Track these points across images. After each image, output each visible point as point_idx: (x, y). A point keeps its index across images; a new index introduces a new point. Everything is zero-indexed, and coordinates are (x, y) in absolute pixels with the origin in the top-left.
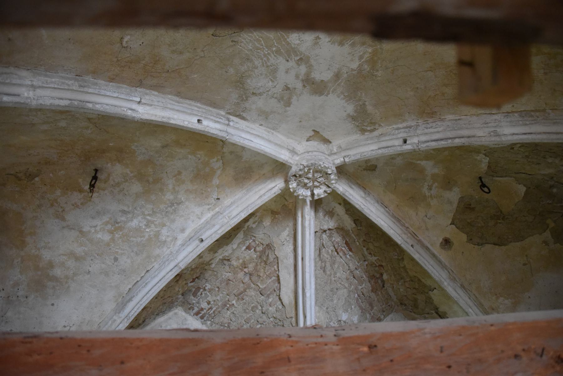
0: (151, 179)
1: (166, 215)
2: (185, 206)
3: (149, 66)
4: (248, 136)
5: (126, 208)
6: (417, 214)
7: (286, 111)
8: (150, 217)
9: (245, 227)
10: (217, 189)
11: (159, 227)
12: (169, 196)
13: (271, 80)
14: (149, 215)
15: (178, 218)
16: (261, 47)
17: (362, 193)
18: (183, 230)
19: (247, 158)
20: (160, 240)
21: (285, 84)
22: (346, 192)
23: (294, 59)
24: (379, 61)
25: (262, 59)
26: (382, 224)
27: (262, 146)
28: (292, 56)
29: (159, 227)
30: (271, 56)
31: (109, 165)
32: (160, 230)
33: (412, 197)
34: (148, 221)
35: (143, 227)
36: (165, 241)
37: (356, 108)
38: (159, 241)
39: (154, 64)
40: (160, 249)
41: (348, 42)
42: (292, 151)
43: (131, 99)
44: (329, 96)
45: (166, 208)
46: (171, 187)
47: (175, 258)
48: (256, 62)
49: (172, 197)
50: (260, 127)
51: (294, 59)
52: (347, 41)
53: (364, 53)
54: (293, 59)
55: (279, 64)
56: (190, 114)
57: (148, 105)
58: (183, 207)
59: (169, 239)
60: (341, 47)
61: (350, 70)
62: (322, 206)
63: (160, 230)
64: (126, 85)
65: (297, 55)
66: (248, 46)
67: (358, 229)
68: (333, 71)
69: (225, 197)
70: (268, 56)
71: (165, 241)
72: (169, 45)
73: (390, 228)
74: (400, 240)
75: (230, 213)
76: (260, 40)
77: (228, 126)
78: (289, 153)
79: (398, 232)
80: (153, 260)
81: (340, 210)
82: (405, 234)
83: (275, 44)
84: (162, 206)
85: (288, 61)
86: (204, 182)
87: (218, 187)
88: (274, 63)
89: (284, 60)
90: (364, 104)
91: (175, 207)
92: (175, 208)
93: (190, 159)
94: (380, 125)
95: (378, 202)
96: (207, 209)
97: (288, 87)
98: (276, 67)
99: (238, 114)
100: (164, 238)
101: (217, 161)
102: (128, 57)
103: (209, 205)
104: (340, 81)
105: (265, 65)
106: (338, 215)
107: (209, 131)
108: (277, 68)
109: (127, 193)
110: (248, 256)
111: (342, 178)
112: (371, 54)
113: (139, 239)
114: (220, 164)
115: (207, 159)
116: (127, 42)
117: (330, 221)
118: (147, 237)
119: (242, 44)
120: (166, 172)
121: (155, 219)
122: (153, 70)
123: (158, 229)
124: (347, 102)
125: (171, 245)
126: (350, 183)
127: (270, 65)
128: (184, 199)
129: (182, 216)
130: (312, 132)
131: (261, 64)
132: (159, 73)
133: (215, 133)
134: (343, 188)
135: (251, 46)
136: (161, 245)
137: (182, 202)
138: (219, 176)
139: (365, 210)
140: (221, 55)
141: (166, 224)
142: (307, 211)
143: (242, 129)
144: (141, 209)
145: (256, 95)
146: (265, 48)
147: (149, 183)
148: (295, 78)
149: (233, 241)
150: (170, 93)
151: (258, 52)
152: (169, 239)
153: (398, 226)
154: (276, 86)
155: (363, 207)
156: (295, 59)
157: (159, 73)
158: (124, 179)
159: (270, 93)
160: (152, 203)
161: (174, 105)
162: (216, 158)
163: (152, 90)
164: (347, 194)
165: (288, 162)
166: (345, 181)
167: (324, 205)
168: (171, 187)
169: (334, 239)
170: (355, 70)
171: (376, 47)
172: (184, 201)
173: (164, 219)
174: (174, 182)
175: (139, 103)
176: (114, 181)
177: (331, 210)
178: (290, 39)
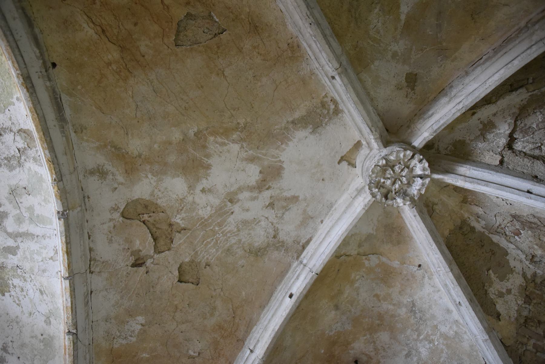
0: (378, 322)
1: (424, 321)
2: (418, 300)
3: (224, 334)
4: (325, 244)
5: (405, 353)
6: (507, 5)
7: (305, 200)
8: (421, 336)
9: (484, 232)
10: (405, 264)
11: (437, 332)
12: (403, 311)
13: (258, 223)
14: (419, 335)
15: (431, 311)
16: (214, 240)
17: (444, 100)
18: (449, 311)
19: (373, 229)
20: (452, 337)
21: (264, 208)
22: (432, 128)
23: (230, 207)
24: (225, 126)
25: (229, 237)
26: (497, 79)
27: (338, 234)
28: (226, 210)
29: (437, 332)
30: (226, 230)
31: (352, 352)
32: (440, 332)
33: (472, 15)
34: (426, 339)
35: (431, 346)
36: (456, 332)
37: (299, 128)
38: (454, 338)
39: (222, 329)
40: (463, 341)
41: (204, 161)
42: (358, 193)
43: (246, 358)
44: (282, 160)
45: (416, 318)
46: (391, 307)
47: (475, 336)
48: (232, 242)
49: (404, 310)
50: (324, 223)
51: (230, 207)
52: (204, 163)
53: (217, 143)
54: (231, 208)
55: (236, 221)
56: (281, 304)
57: (256, 344)
58: (418, 303)
59: (455, 328)
60: (213, 166)
61: (242, 149)
62: (468, 141)
63: (440, 332)
64: (239, 353)
65: (226, 206)
66: (213, 252)
67: (533, 82)
68: (246, 165)
69: (419, 258)
70: (226, 232)
71: (456, 332)
72: (205, 318)
73: (509, 65)
74: (537, 50)
75: (434, 265)
76: (206, 243)
77: (307, 265)
78: (360, 196)
79: (525, 48)
80: (475, 353)
81: (485, 113)
82: (533, 34)
83: (212, 228)
84: (412, 321)
85: (232, 213)
86: (394, 275)
87: (403, 263)
88: (234, 225)
89: (231, 216)
90: (293, 122)
91: (417, 309)
92: (418, 310)
93: (360, 284)
94: (326, 96)
95: (467, 74)
96: (429, 280)
97: (268, 204)
98: (240, 223)
99: (301, 248)
100: (452, 332)
101: (369, 260)
102: (210, 351)
103: (424, 277)
104: (259, 155)
105: (236, 234)
106: (495, 115)
107: (300, 291)
108: (241, 221)
109: (388, 346)
110: (529, 239)
111: (414, 128)
112: (217, 136)
113: (444, 355)
114: (373, 258)
115: (364, 270)
116: (194, 353)
117: (498, 132)
118: (444, 347)
119: (210, 257)
120: (373, 307)
121: (426, 332)
122: (229, 330)
123: (439, 334)
124: (291, 140)
125: (463, 329)
126: (425, 117)
127: (237, 228)
128: (410, 299)
129: (430, 307)
130: (341, 164)
131: (235, 237)
132: (233, 325)
133: (305, 286)
134: (426, 131)
135: (213, 250)
136: (459, 338)
137: (413, 301)
138: (390, 260)
139: (466, 103)
140: (221, 274)
141: (435, 324)
142: (451, 181)
143: (314, 251)
144: (409, 340)
145: (278, 234)
146: (216, 236)
147: (381, 324)
148: (256, 201)
149: (503, 246)
150: (259, 314)
151: (220, 242)
152: (455, 328)
153: (514, 47)
154: (267, 217)
155: (461, 106)
156: (230, 206)
157: (233, 325)
158: (371, 343)
159: (275, 221)
160: (406, 328)
161: (267, 317)
162: (364, 261)
163: (251, 330)
164: (435, 127)
165: (367, 203)
166: (420, 123)
167: (468, 138)
168: (391, 307)
169: (534, 126)
170: (242, 145)
171: (206, 134)
172: (412, 300)
173: (428, 324)
174: (385, 302)
175: (252, 351)
176: (371, 351)
177: (481, 126)
178: (205, 216)
